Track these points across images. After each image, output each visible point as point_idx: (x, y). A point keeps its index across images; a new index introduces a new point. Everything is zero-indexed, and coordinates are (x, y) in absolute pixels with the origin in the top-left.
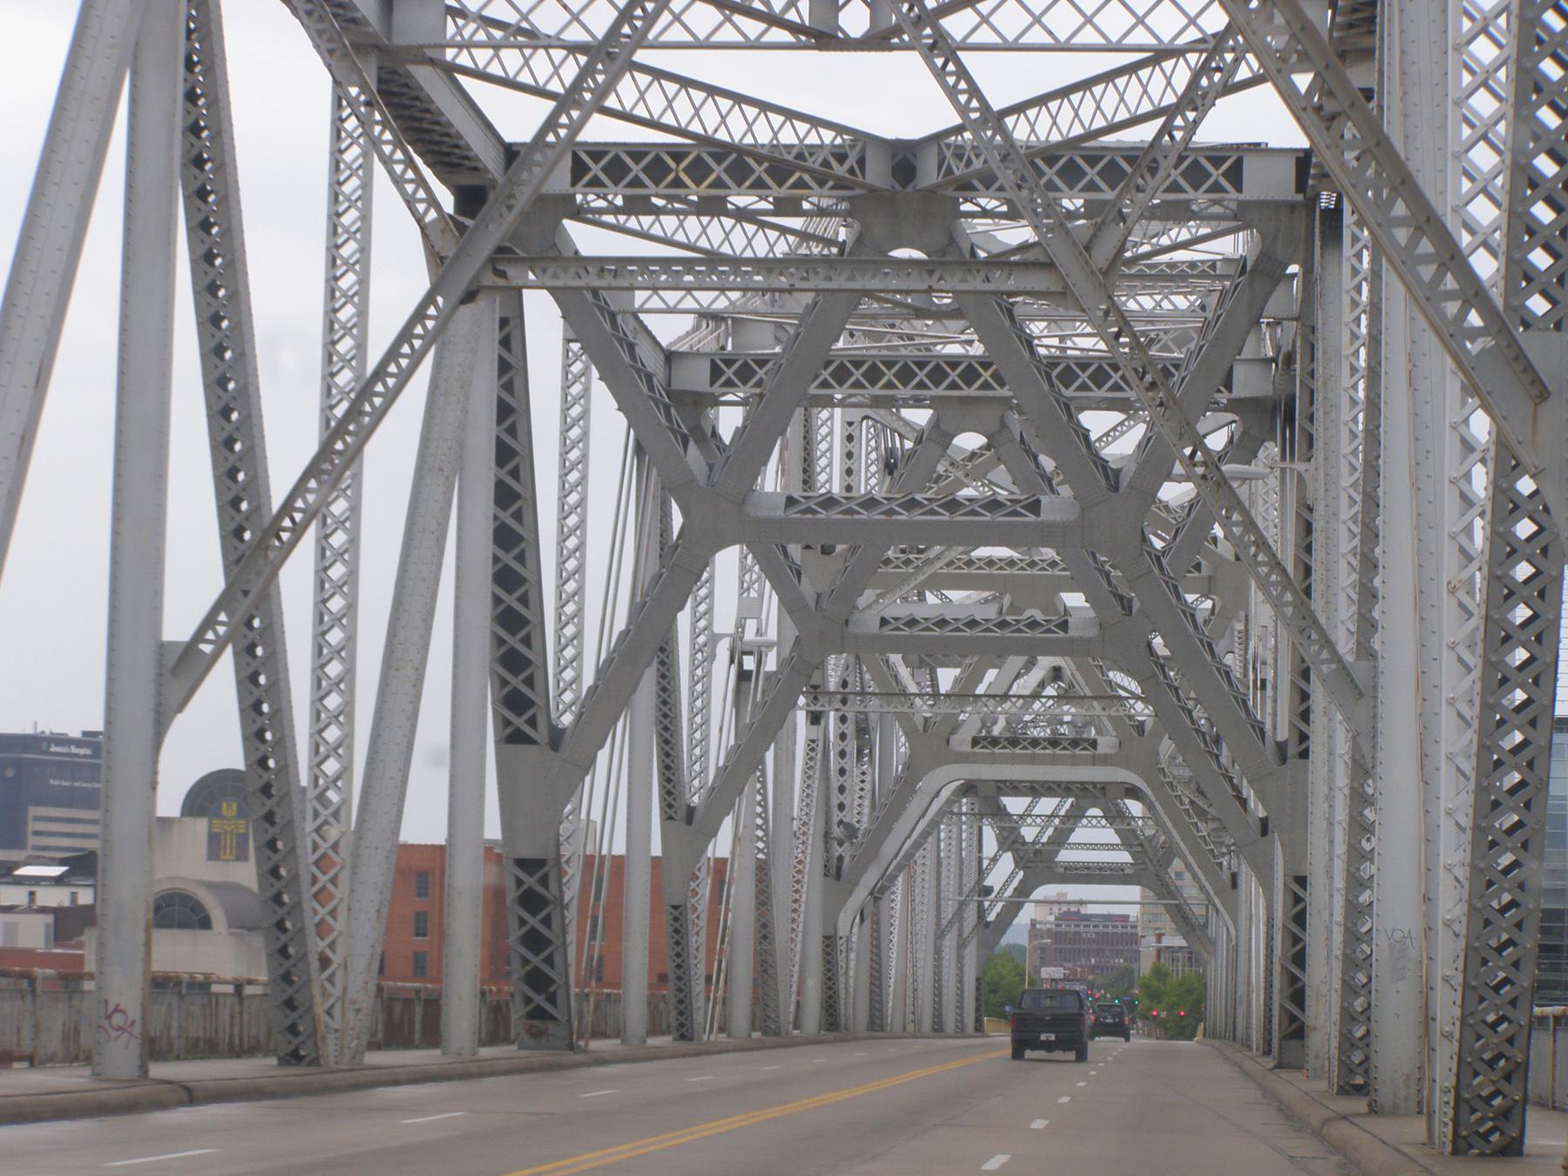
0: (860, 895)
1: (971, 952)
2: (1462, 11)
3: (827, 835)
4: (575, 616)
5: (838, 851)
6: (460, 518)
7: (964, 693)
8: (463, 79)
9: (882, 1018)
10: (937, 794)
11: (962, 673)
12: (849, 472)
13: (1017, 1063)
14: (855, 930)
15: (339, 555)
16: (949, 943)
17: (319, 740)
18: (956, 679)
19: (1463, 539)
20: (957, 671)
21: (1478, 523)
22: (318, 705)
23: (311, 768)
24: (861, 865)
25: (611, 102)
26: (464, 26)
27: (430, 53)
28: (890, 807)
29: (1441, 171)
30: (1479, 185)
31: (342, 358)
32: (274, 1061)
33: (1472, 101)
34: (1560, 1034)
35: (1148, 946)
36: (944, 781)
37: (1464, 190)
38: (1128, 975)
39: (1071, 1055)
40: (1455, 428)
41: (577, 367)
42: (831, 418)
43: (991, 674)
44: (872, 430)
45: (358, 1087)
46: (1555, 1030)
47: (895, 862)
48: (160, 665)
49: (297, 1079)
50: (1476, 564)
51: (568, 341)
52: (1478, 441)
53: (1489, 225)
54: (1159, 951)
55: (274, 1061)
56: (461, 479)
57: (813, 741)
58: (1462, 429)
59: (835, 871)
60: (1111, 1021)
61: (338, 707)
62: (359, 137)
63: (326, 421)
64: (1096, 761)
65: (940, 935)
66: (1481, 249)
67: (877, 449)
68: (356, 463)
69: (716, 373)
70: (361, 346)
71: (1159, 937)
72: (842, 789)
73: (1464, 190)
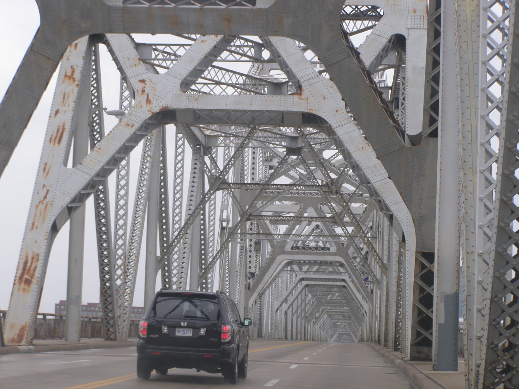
0: (255, 295)
2: (486, 43)
3: (246, 276)
5: (249, 281)
6: (148, 212)
7: (287, 234)
8: (157, 68)
9: (261, 334)
10: (280, 263)
11: (289, 226)
12: (253, 174)
14: (254, 306)
18: (287, 228)
19: (487, 174)
20: (287, 226)
21: (495, 166)
22: (116, 233)
24: (256, 285)
27: (147, 61)
28: (265, 270)
29: (476, 64)
32: (103, 339)
33: (492, 35)
36: (282, 259)
37: (488, 54)
40: (481, 200)
41: (180, 143)
42: (249, 150)
43: (297, 227)
44: (261, 151)
47: (266, 285)
50: (493, 186)
51: (177, 134)
55: (103, 339)
57: (242, 247)
58: (487, 146)
59: (248, 287)
60: (189, 333)
66: (495, 109)
67: (262, 157)
72: (250, 257)
73: (488, 54)
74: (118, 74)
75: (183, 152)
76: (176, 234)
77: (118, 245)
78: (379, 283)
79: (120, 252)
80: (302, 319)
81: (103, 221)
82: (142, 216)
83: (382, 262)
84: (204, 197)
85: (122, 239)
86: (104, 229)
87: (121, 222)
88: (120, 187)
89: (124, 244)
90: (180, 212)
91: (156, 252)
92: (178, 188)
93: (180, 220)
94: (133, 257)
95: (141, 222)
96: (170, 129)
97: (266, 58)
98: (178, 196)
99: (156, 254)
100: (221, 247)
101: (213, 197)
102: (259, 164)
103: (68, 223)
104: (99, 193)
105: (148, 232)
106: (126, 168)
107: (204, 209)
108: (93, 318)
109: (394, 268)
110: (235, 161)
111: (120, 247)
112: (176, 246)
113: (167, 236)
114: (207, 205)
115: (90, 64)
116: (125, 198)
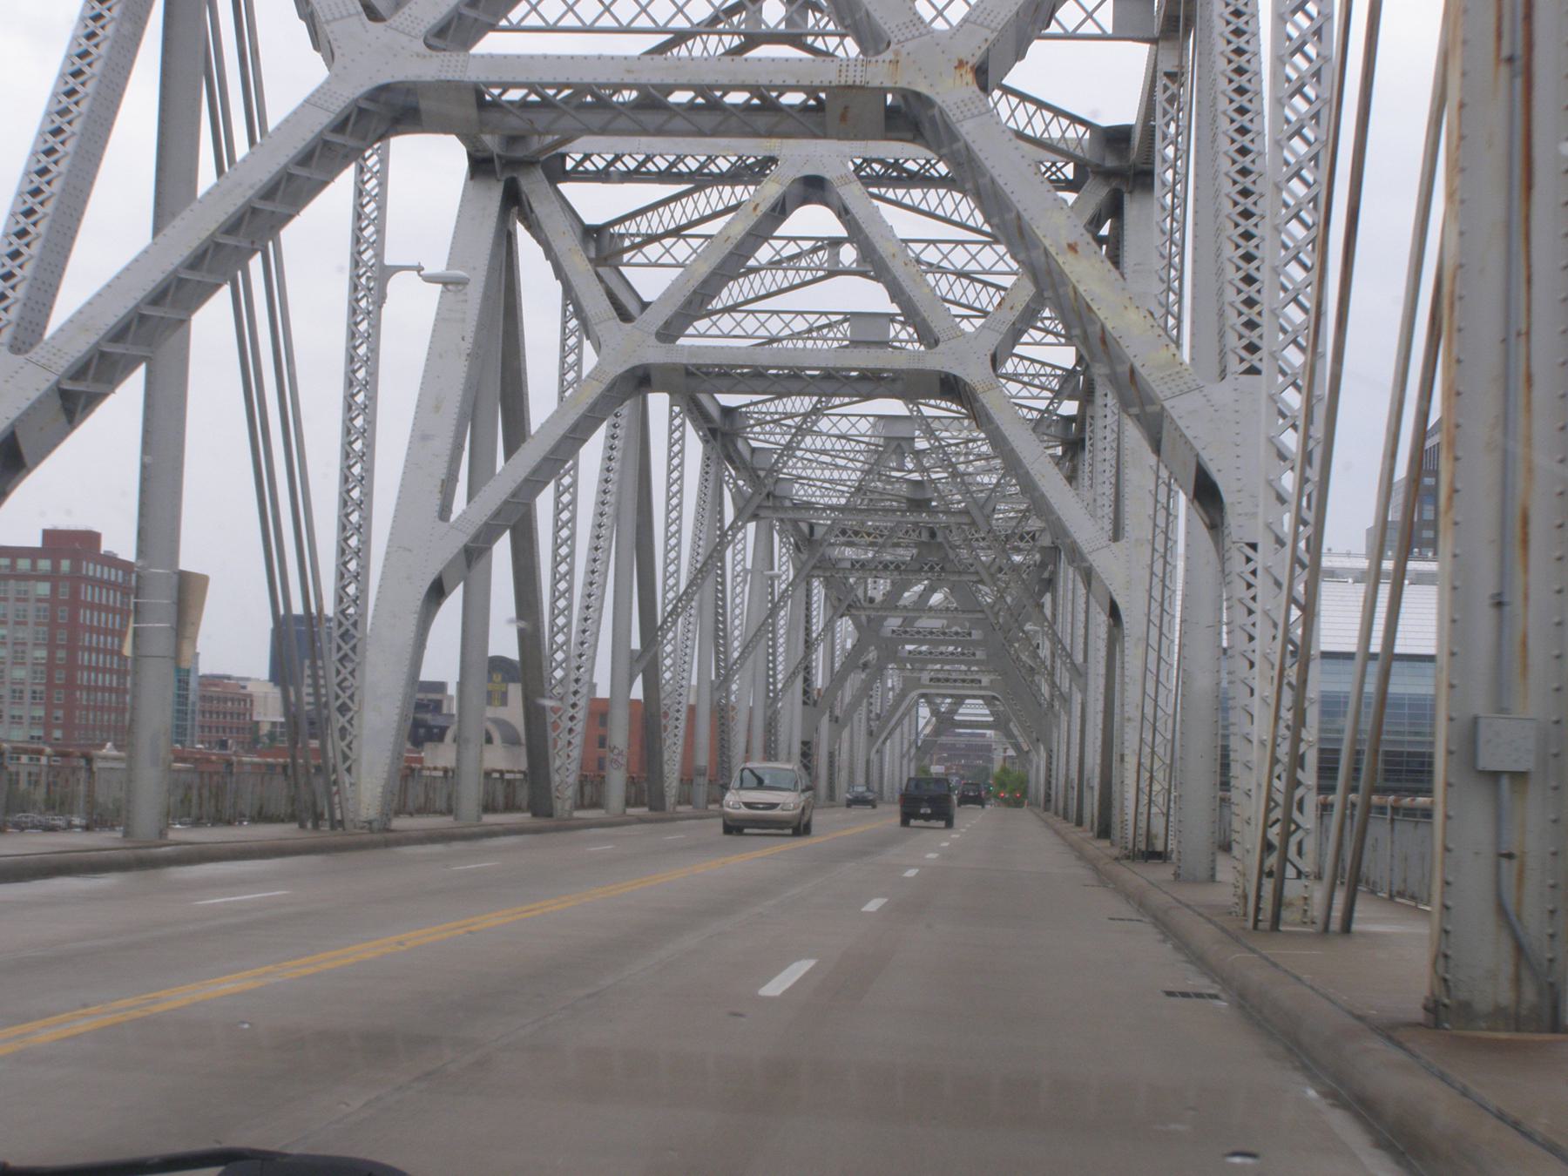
1: (913, 765)
13: (906, 829)
16: (905, 762)
19: (1161, 249)
25: (803, 446)
26: (821, 19)
34: (1398, 826)
35: (998, 757)
38: (985, 771)
39: (942, 824)
41: (677, 422)
45: (387, 844)
46: (1392, 820)
48: (631, 658)
49: (126, 852)
51: (671, 406)
54: (1005, 759)
64: (981, 688)
65: (902, 757)
69: (853, 565)
71: (1005, 750)
74: (558, 286)
75: (682, 437)
76: (669, 608)
78: (1065, 700)
79: (559, 656)
80: (910, 760)
83: (1073, 663)
84: (724, 535)
87: (561, 621)
89: (567, 642)
90: (677, 571)
92: (673, 541)
93: (677, 584)
96: (658, 403)
98: (673, 555)
101: (740, 536)
103: (461, 586)
105: (616, 564)
107: (722, 560)
108: (508, 772)
109: (1098, 668)
110: (793, 591)
111: (560, 647)
112: (669, 629)
114: (729, 553)
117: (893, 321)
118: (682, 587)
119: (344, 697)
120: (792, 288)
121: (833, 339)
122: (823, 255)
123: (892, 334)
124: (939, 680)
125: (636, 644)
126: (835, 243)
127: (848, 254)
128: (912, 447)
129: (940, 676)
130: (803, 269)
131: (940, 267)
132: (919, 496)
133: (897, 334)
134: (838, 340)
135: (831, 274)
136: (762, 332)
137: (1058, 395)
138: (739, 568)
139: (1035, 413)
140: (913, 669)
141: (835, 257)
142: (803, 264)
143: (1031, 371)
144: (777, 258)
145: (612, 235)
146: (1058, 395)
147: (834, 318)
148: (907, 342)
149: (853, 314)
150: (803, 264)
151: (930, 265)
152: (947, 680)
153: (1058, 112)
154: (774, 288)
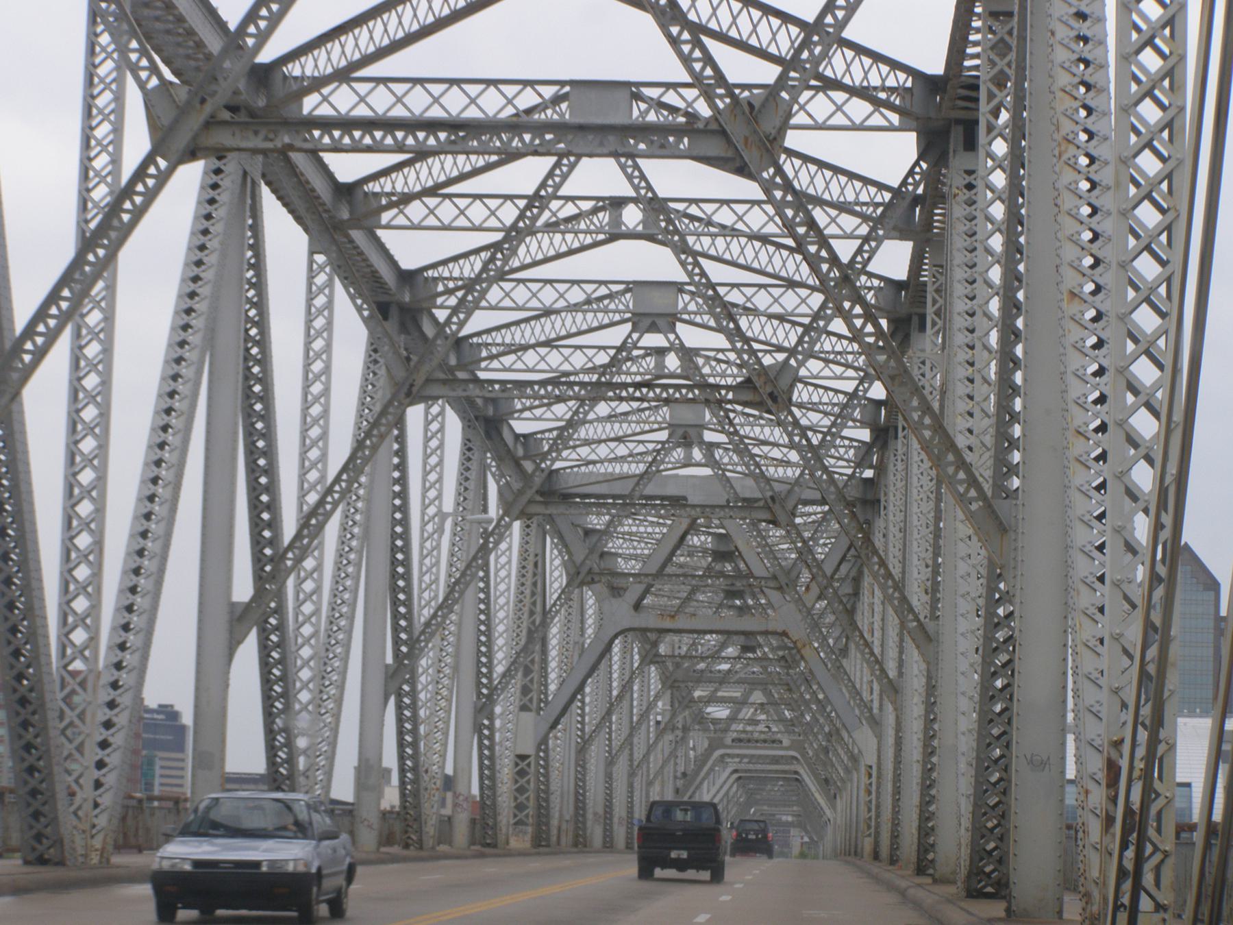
4: (320, 439)
15: (87, 493)
17: (69, 578)
23: (59, 638)
30: (1144, 294)
31: (90, 330)
39: (706, 875)
51: (312, 253)
52: (1142, 437)
53: (1156, 175)
55: (20, 862)
56: (212, 356)
61: (91, 483)
62: (113, 52)
63: (81, 232)
66: (1144, 305)
68: (111, 268)
70: (116, 161)
75: (441, 429)
77: (303, 614)
79: (306, 652)
81: (262, 462)
82: (331, 740)
84: (486, 542)
85: (312, 624)
86: (259, 425)
88: (306, 485)
89: (317, 612)
91: (384, 654)
94: (330, 705)
95: (333, 725)
97: (631, 207)
99: (379, 804)
100: (359, 446)
102: (551, 563)
104: (251, 364)
106: (324, 357)
113: (408, 617)
115: (243, 236)
116: (321, 422)
117: (681, 291)
118: (441, 599)
119: (70, 715)
120: (571, 252)
121: (614, 312)
122: (604, 217)
123: (681, 305)
124: (740, 740)
125: (243, 589)
126: (617, 203)
127: (632, 216)
128: (701, 436)
129: (743, 736)
130: (582, 232)
131: (734, 229)
132: (723, 548)
133: (686, 305)
134: (620, 312)
135: (613, 238)
136: (534, 303)
137: (866, 379)
138: (432, 510)
139: (841, 396)
140: (715, 731)
141: (617, 221)
142: (583, 226)
143: (838, 348)
144: (554, 219)
145: (426, 279)
146: (866, 379)
147: (615, 288)
148: (695, 313)
149: (635, 283)
150: (583, 226)
151: (723, 227)
152: (749, 741)
153: (877, 57)
154: (552, 253)
